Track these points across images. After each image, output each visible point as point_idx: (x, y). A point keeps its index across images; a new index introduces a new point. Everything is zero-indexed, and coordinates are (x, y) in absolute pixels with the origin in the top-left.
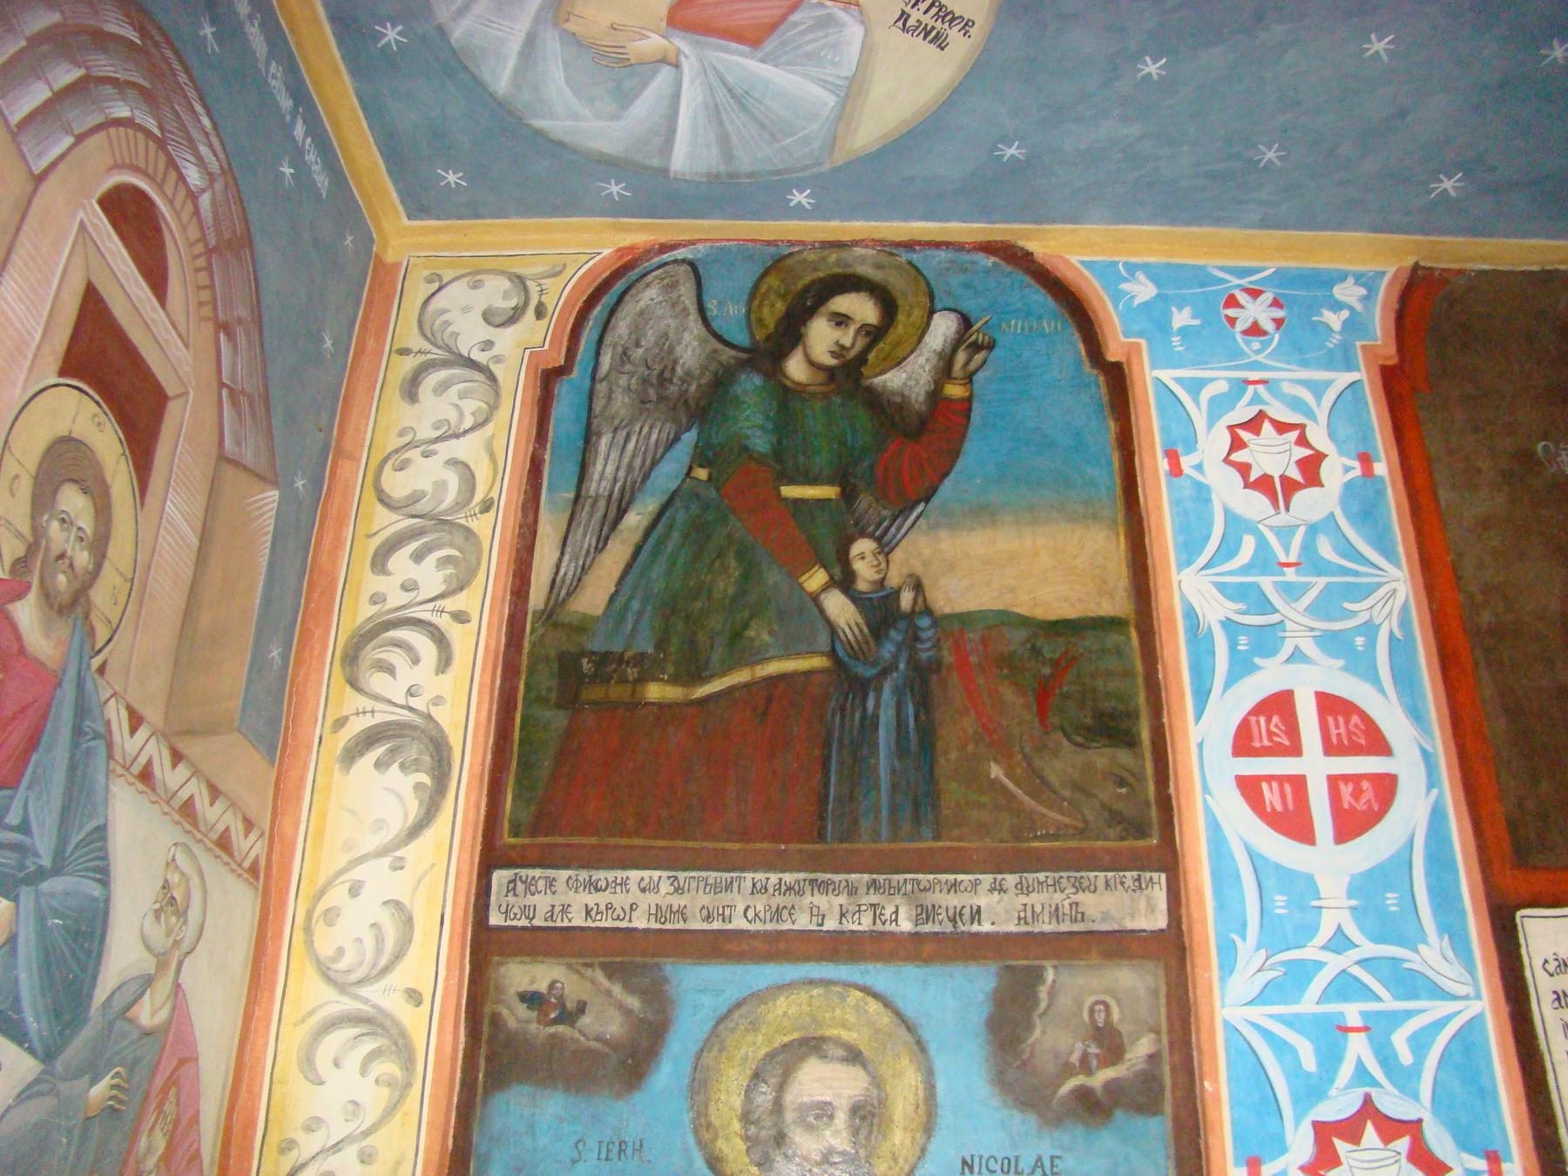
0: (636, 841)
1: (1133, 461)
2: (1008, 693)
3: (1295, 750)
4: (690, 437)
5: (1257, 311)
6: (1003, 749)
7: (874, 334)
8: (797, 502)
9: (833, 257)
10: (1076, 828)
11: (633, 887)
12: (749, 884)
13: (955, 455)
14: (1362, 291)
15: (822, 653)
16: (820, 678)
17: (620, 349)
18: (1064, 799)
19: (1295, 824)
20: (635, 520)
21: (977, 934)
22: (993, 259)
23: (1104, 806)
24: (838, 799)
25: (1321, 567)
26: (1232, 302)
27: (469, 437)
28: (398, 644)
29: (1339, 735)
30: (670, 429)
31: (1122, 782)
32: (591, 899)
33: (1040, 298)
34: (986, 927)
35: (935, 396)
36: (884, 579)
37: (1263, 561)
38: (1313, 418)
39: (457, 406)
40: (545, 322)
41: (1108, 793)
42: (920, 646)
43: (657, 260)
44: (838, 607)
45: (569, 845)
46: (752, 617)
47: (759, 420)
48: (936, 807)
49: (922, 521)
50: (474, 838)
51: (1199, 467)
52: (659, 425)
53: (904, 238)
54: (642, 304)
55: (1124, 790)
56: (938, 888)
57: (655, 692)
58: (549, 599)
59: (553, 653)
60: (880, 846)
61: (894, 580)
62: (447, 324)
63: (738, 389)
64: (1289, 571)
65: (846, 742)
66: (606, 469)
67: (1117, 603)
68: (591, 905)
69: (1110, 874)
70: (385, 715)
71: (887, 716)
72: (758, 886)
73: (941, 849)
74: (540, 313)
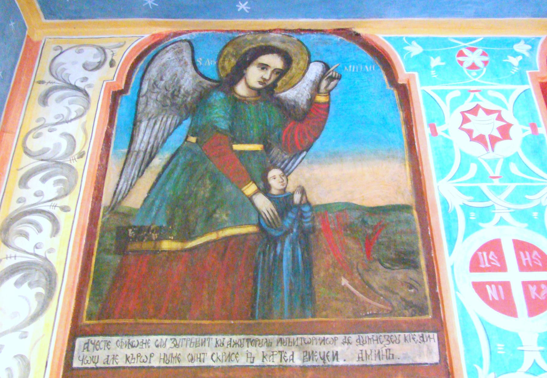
0: (155, 321)
1: (412, 130)
2: (351, 243)
3: (503, 268)
4: (187, 123)
5: (475, 58)
6: (347, 269)
7: (280, 73)
8: (241, 152)
9: (260, 38)
10: (388, 310)
11: (152, 345)
12: (214, 342)
13: (321, 129)
14: (529, 47)
15: (254, 225)
16: (252, 236)
17: (152, 82)
18: (381, 295)
19: (506, 306)
20: (158, 162)
21: (336, 366)
22: (340, 38)
23: (403, 299)
24: (262, 298)
25: (512, 179)
26: (461, 54)
27: (73, 122)
28: (31, 222)
29: (527, 261)
30: (177, 118)
31: (411, 287)
32: (129, 351)
33: (365, 56)
34: (341, 362)
35: (311, 101)
36: (285, 189)
37: (481, 176)
38: (505, 107)
39: (67, 108)
40: (114, 69)
41: (404, 292)
42: (304, 220)
43: (172, 40)
44: (263, 203)
45: (118, 324)
46: (218, 207)
47: (222, 114)
48: (313, 301)
49: (305, 160)
50: (67, 320)
51: (446, 132)
52: (172, 116)
53: (296, 28)
54: (164, 61)
55: (412, 291)
56: (315, 342)
57: (166, 245)
58: (112, 201)
59: (113, 226)
60: (284, 321)
61: (291, 188)
62: (65, 69)
63: (212, 100)
64: (496, 180)
65: (266, 268)
66: (144, 139)
67: (406, 197)
68: (129, 354)
69: (407, 334)
70: (22, 258)
71: (287, 255)
72: (219, 343)
73: (317, 322)
74: (112, 64)
